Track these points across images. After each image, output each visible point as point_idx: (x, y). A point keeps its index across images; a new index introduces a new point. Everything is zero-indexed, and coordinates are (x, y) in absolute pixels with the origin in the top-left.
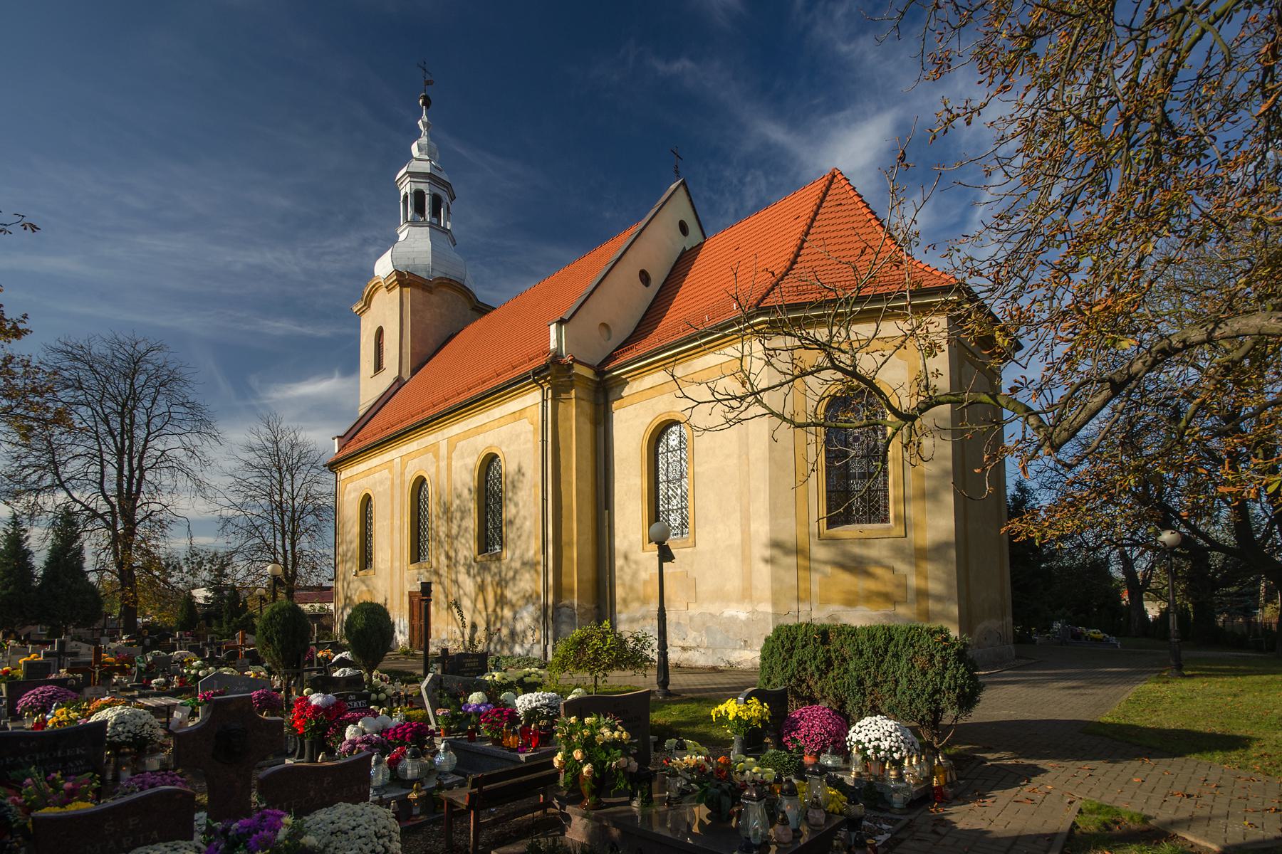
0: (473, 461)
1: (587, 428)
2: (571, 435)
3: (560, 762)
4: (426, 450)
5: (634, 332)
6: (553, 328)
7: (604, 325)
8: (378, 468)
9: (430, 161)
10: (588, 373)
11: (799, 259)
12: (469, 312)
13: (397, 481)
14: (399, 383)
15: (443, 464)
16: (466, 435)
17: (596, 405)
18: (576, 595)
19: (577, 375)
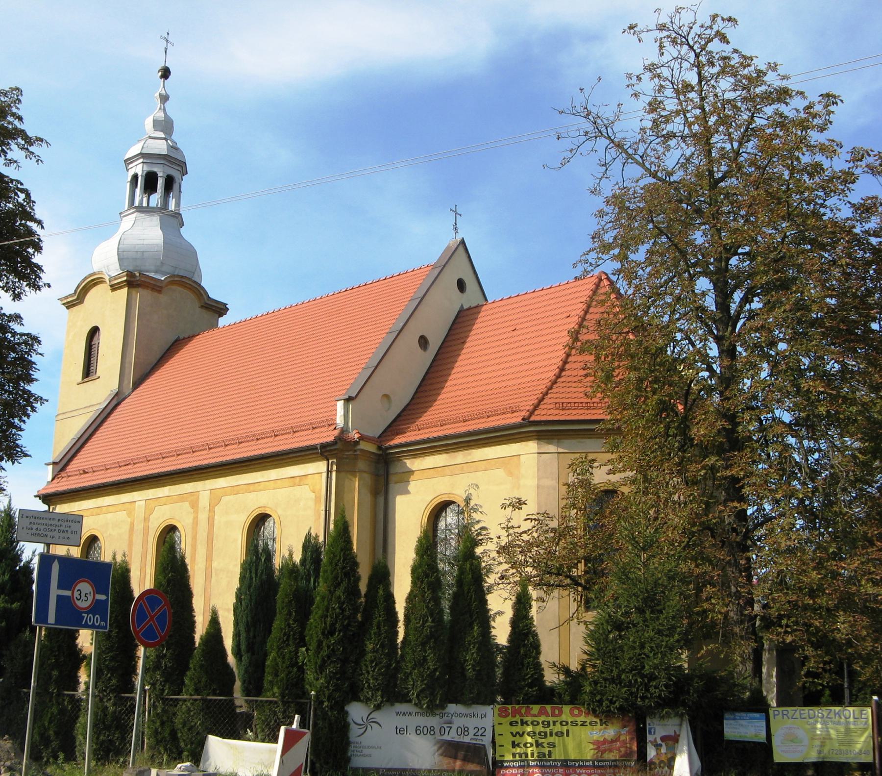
0: (241, 521)
1: (368, 498)
2: (354, 506)
3: (729, 424)
4: (182, 498)
5: (413, 398)
6: (340, 405)
7: (386, 396)
8: (111, 508)
9: (166, 139)
10: (371, 448)
11: (567, 366)
12: (198, 310)
13: (138, 527)
14: (117, 400)
15: (203, 516)
16: (235, 490)
17: (376, 476)
18: (140, 663)
19: (362, 450)
